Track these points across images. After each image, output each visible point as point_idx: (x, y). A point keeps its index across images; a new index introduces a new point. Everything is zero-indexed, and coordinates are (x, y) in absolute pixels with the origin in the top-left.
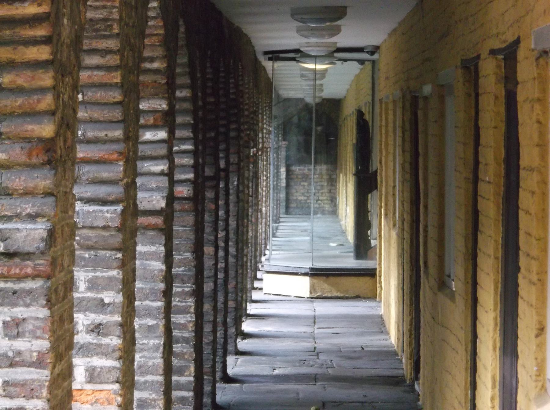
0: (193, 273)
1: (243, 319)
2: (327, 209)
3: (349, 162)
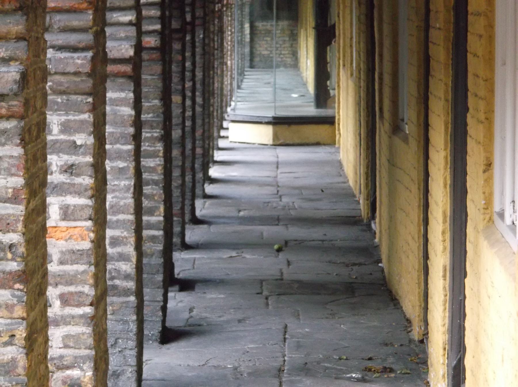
0: (161, 119)
1: (211, 165)
2: (289, 62)
3: (310, 17)
